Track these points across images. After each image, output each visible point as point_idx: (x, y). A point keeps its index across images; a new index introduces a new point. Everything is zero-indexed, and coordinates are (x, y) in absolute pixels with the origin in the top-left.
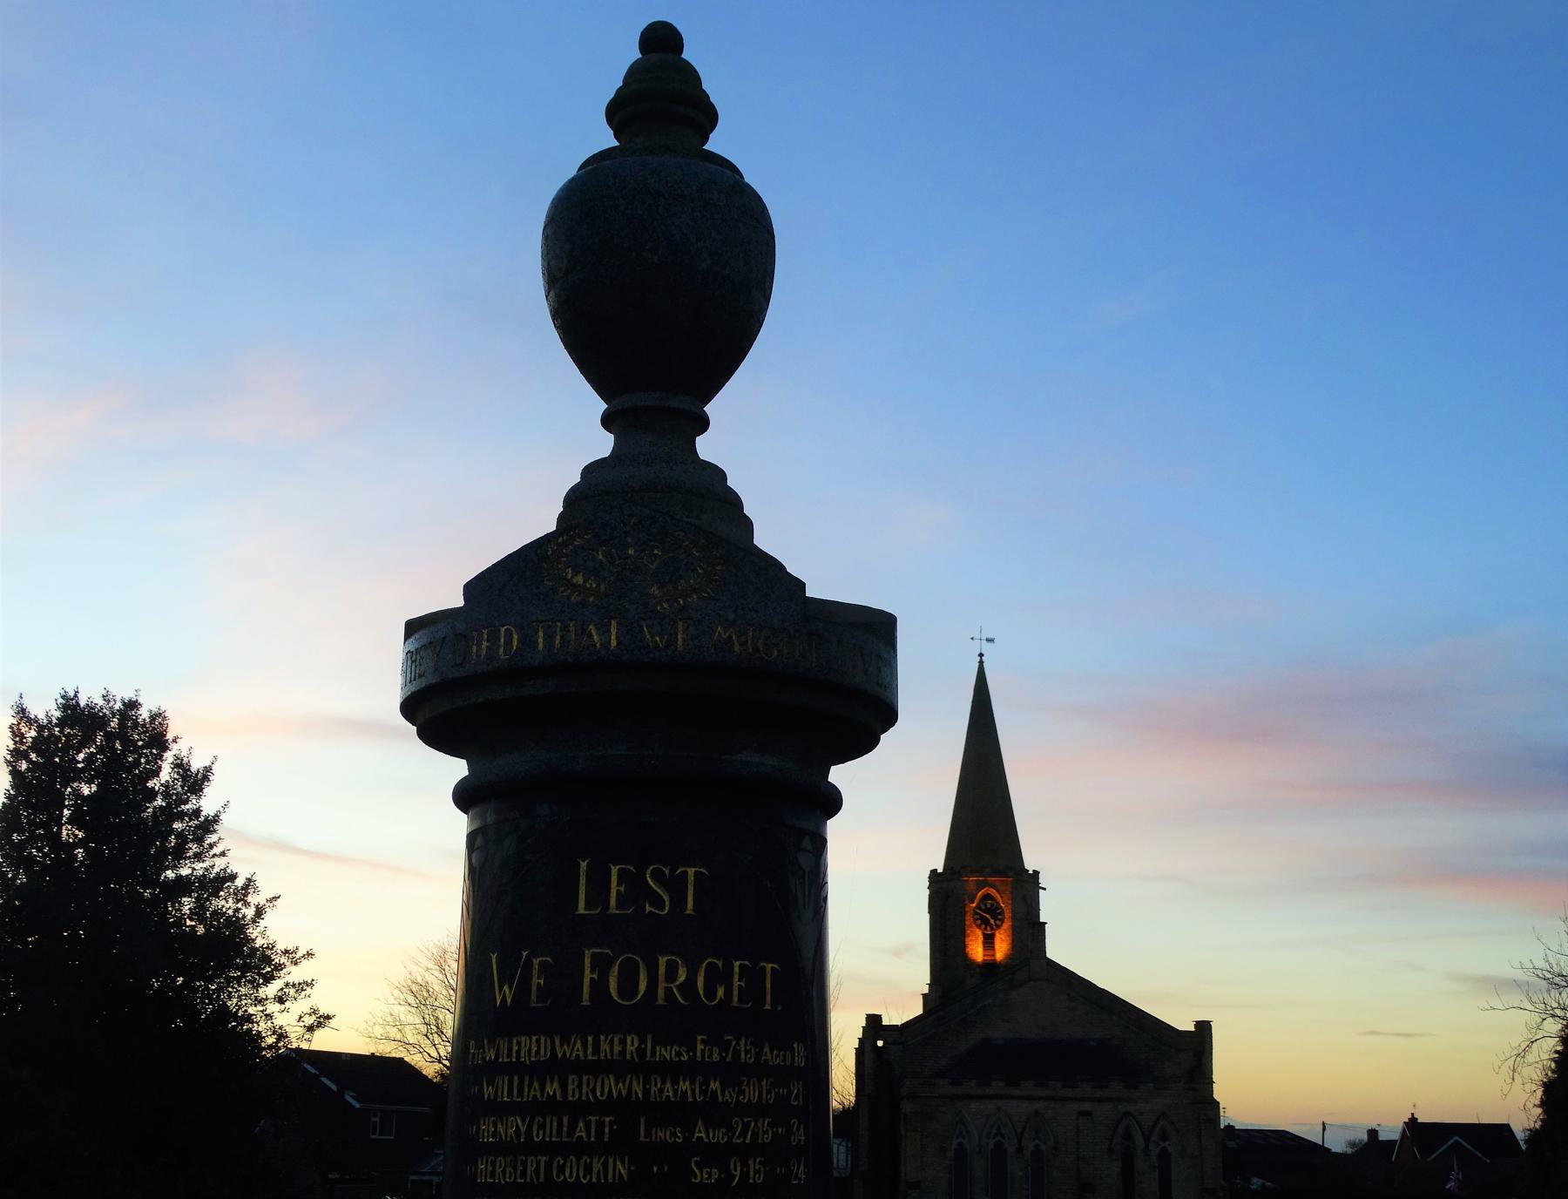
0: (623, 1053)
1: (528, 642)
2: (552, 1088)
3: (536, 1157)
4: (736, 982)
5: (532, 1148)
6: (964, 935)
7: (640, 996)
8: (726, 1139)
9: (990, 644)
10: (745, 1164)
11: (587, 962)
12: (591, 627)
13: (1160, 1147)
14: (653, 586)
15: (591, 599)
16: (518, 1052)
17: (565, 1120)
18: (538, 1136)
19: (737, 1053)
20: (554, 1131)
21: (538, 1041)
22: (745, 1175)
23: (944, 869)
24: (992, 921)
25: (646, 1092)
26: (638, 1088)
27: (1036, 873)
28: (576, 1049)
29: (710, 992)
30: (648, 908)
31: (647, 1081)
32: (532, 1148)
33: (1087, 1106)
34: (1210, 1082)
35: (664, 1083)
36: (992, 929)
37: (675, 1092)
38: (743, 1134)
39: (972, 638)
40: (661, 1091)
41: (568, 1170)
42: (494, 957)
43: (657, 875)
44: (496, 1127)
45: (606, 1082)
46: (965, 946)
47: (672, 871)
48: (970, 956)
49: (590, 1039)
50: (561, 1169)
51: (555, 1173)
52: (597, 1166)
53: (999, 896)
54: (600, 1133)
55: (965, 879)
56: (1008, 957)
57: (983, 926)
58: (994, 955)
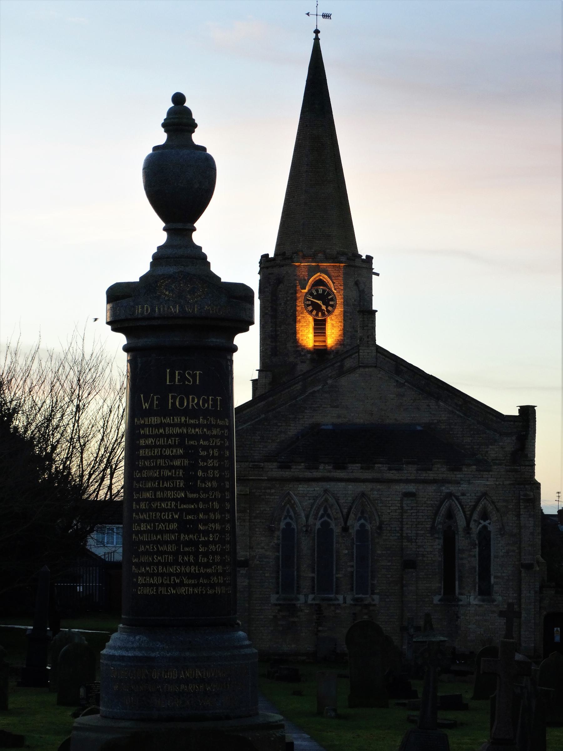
0: (181, 421)
1: (153, 310)
2: (161, 431)
3: (164, 444)
4: (210, 402)
5: (156, 446)
6: (294, 321)
7: (185, 407)
8: (208, 444)
9: (327, 20)
10: (213, 451)
11: (170, 397)
12: (171, 307)
13: (480, 526)
14: (188, 295)
15: (171, 299)
16: (151, 421)
17: (165, 439)
18: (158, 443)
19: (211, 422)
20: (162, 442)
21: (157, 418)
22: (213, 454)
23: (275, 255)
24: (324, 307)
25: (187, 432)
26: (185, 431)
27: (369, 259)
28: (168, 420)
29: (204, 405)
30: (186, 383)
31: (187, 429)
32: (156, 446)
33: (411, 488)
34: (532, 465)
35: (192, 429)
36: (323, 314)
37: (195, 431)
38: (213, 443)
39: (308, 14)
40: (191, 431)
41: (166, 452)
42: (142, 396)
43: (189, 374)
44: (145, 442)
45: (176, 429)
46: (295, 333)
47: (193, 372)
48: (300, 342)
49: (172, 418)
50: (165, 452)
51: (163, 453)
52: (174, 451)
53: (330, 282)
54: (175, 443)
55: (297, 264)
56: (341, 343)
57: (314, 312)
58: (325, 341)
